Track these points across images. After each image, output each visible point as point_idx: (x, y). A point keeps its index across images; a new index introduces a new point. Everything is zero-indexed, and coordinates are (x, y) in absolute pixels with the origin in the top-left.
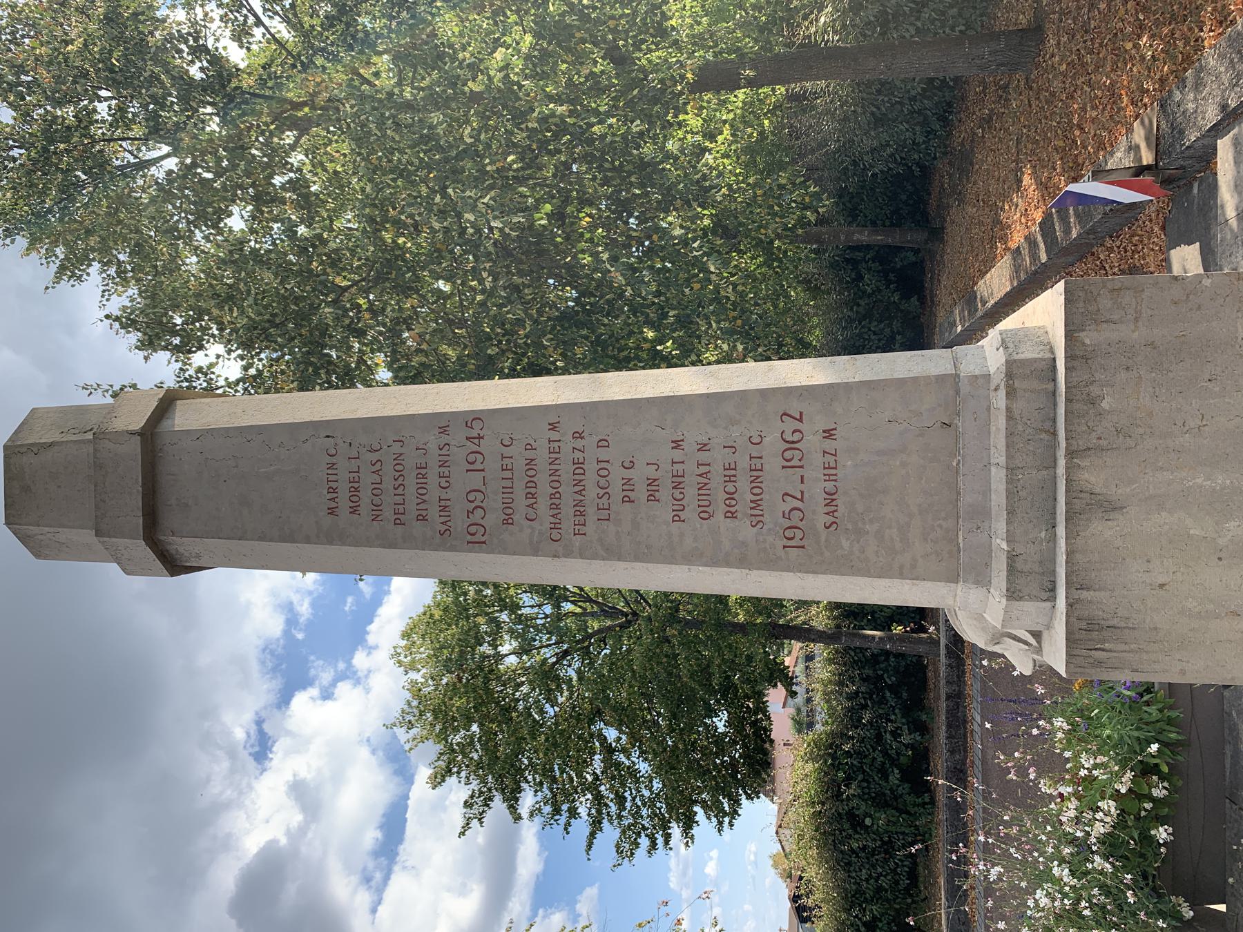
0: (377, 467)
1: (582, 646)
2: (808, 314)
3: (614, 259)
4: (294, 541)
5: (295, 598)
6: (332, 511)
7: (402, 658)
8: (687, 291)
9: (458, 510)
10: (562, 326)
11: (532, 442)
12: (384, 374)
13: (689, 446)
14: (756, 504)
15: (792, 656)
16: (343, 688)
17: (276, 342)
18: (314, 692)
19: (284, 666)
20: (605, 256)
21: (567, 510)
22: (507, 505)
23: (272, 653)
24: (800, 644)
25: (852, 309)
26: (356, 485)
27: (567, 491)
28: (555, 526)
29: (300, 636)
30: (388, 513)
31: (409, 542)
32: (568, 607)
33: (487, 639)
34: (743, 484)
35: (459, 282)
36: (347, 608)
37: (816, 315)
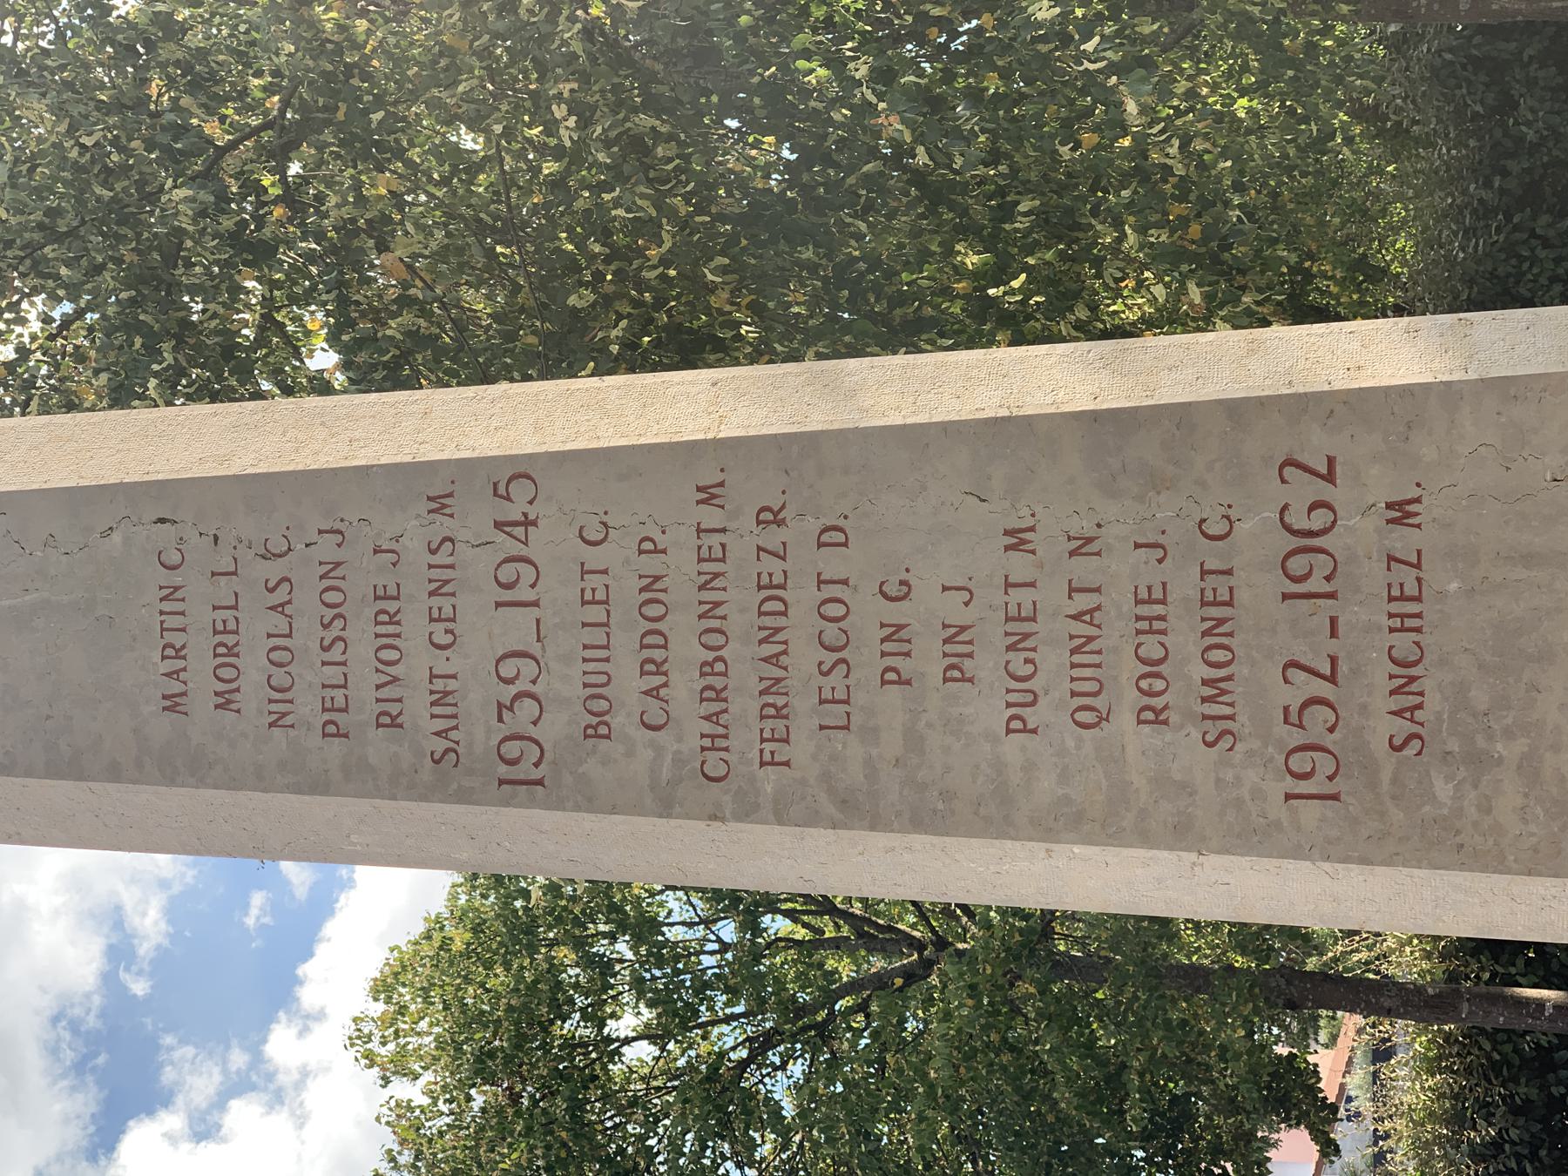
0: (281, 595)
1: (804, 1025)
2: (1376, 195)
3: (884, 76)
4: (80, 777)
5: (128, 897)
6: (173, 704)
7: (374, 1045)
8: (1065, 151)
9: (477, 697)
10: (752, 238)
11: (656, 534)
12: (323, 359)
13: (1049, 542)
14: (1216, 689)
15: (1336, 1056)
16: (242, 1114)
17: (57, 277)
18: (173, 1120)
19: (101, 1060)
20: (861, 70)
21: (744, 705)
22: (596, 690)
23: (75, 1027)
24: (1359, 1020)
25: (1488, 184)
26: (230, 640)
27: (742, 657)
28: (714, 743)
29: (139, 988)
30: (307, 705)
31: (357, 779)
32: (776, 925)
33: (580, 1001)
34: (1185, 638)
35: (498, 129)
36: (250, 921)
37: (1400, 197)
